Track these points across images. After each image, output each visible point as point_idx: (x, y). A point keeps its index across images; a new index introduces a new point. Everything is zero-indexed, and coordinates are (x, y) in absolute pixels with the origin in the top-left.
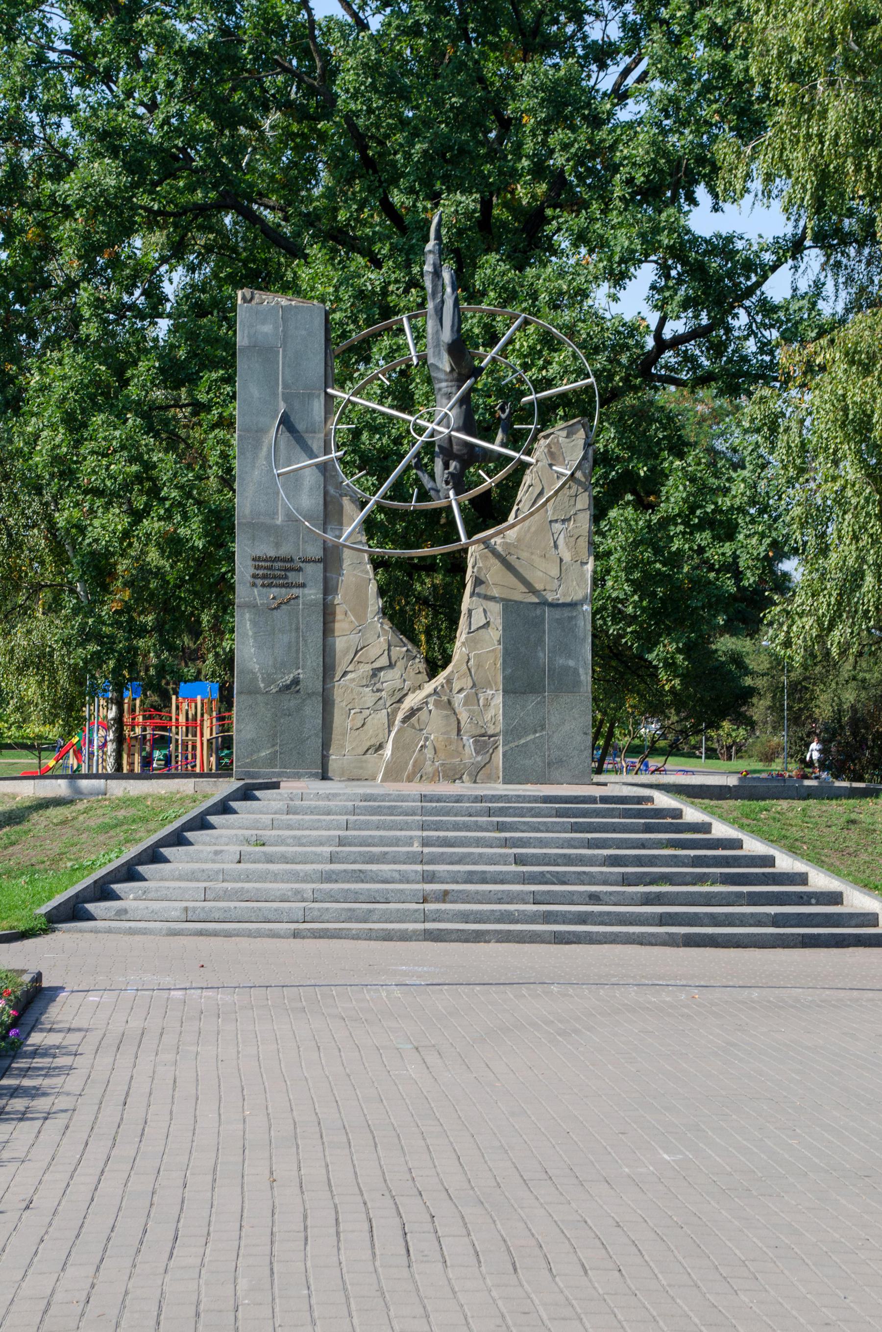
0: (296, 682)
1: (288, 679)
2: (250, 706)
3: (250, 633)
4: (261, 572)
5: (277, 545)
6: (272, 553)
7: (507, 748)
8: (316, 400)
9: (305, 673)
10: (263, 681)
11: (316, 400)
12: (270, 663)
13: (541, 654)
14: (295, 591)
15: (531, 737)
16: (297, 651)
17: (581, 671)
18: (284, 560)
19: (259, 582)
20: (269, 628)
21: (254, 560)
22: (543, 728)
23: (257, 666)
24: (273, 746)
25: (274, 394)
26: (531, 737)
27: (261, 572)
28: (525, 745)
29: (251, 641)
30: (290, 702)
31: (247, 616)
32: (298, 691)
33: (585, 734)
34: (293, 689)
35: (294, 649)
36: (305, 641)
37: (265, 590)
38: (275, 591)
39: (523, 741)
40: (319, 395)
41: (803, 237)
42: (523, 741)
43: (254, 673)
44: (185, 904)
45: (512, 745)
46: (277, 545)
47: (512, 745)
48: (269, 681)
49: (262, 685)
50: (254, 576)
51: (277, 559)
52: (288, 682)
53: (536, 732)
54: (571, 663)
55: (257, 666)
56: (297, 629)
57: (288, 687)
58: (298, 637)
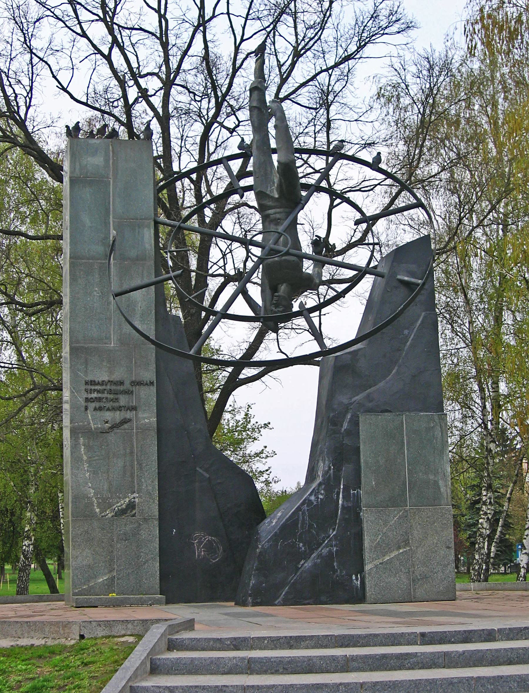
0: (131, 506)
1: (123, 503)
2: (87, 532)
3: (85, 458)
8: (146, 229)
9: (140, 497)
10: (98, 507)
11: (146, 229)
12: (106, 487)
15: (396, 553)
16: (132, 475)
17: (441, 483)
18: (115, 383)
19: (92, 406)
20: (103, 452)
21: (86, 383)
22: (407, 543)
24: (111, 571)
25: (106, 224)
26: (396, 553)
27: (95, 395)
28: (391, 561)
29: (86, 466)
30: (126, 525)
31: (82, 440)
32: (134, 515)
33: (448, 547)
35: (128, 474)
36: (140, 465)
37: (98, 413)
38: (108, 415)
39: (387, 558)
40: (149, 228)
41: (59, 573)
42: (387, 558)
43: (88, 498)
44: (67, 235)
46: (111, 373)
48: (105, 504)
49: (98, 510)
50: (87, 400)
52: (124, 506)
53: (399, 548)
56: (132, 453)
58: (132, 461)
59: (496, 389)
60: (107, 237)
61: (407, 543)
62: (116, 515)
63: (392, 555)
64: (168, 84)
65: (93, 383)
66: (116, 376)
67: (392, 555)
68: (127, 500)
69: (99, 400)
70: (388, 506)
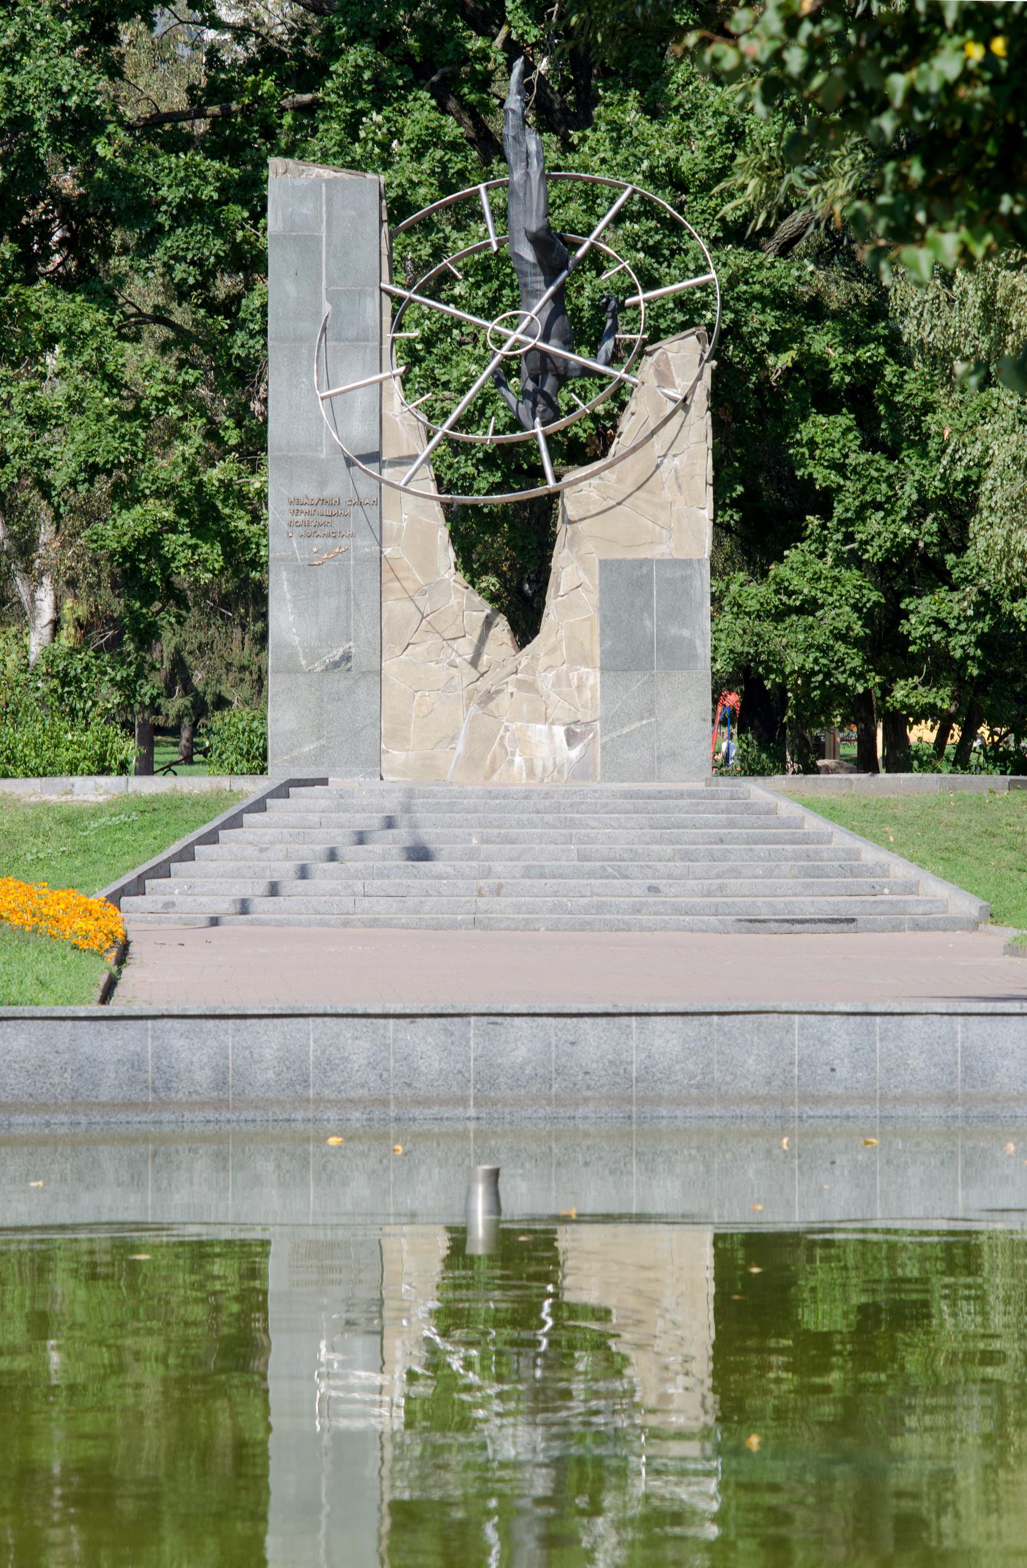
0: (347, 658)
1: (337, 654)
4: (301, 518)
5: (323, 484)
6: (314, 495)
7: (606, 739)
13: (648, 623)
14: (344, 542)
15: (637, 724)
22: (651, 713)
23: (297, 639)
25: (317, 293)
26: (637, 724)
27: (301, 518)
28: (630, 735)
29: (290, 606)
34: (344, 666)
36: (357, 605)
39: (626, 730)
42: (626, 730)
45: (614, 735)
47: (614, 735)
51: (323, 501)
54: (686, 633)
55: (297, 639)
56: (348, 590)
57: (336, 665)
59: (644, 9)
60: (318, 313)
61: (651, 713)
62: (327, 669)
63: (633, 727)
64: (629, 1101)
65: (298, 502)
66: (328, 492)
67: (633, 727)
68: (341, 650)
69: (307, 524)
70: (628, 670)
